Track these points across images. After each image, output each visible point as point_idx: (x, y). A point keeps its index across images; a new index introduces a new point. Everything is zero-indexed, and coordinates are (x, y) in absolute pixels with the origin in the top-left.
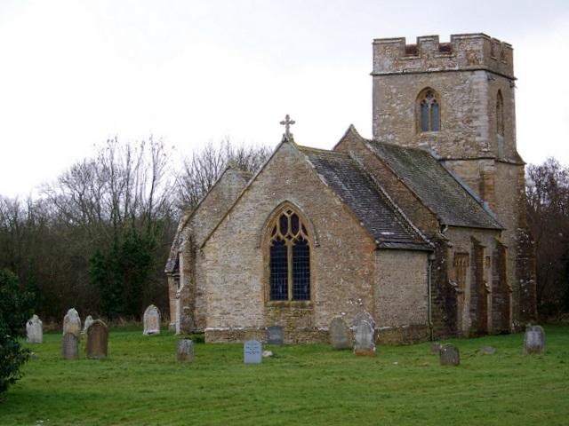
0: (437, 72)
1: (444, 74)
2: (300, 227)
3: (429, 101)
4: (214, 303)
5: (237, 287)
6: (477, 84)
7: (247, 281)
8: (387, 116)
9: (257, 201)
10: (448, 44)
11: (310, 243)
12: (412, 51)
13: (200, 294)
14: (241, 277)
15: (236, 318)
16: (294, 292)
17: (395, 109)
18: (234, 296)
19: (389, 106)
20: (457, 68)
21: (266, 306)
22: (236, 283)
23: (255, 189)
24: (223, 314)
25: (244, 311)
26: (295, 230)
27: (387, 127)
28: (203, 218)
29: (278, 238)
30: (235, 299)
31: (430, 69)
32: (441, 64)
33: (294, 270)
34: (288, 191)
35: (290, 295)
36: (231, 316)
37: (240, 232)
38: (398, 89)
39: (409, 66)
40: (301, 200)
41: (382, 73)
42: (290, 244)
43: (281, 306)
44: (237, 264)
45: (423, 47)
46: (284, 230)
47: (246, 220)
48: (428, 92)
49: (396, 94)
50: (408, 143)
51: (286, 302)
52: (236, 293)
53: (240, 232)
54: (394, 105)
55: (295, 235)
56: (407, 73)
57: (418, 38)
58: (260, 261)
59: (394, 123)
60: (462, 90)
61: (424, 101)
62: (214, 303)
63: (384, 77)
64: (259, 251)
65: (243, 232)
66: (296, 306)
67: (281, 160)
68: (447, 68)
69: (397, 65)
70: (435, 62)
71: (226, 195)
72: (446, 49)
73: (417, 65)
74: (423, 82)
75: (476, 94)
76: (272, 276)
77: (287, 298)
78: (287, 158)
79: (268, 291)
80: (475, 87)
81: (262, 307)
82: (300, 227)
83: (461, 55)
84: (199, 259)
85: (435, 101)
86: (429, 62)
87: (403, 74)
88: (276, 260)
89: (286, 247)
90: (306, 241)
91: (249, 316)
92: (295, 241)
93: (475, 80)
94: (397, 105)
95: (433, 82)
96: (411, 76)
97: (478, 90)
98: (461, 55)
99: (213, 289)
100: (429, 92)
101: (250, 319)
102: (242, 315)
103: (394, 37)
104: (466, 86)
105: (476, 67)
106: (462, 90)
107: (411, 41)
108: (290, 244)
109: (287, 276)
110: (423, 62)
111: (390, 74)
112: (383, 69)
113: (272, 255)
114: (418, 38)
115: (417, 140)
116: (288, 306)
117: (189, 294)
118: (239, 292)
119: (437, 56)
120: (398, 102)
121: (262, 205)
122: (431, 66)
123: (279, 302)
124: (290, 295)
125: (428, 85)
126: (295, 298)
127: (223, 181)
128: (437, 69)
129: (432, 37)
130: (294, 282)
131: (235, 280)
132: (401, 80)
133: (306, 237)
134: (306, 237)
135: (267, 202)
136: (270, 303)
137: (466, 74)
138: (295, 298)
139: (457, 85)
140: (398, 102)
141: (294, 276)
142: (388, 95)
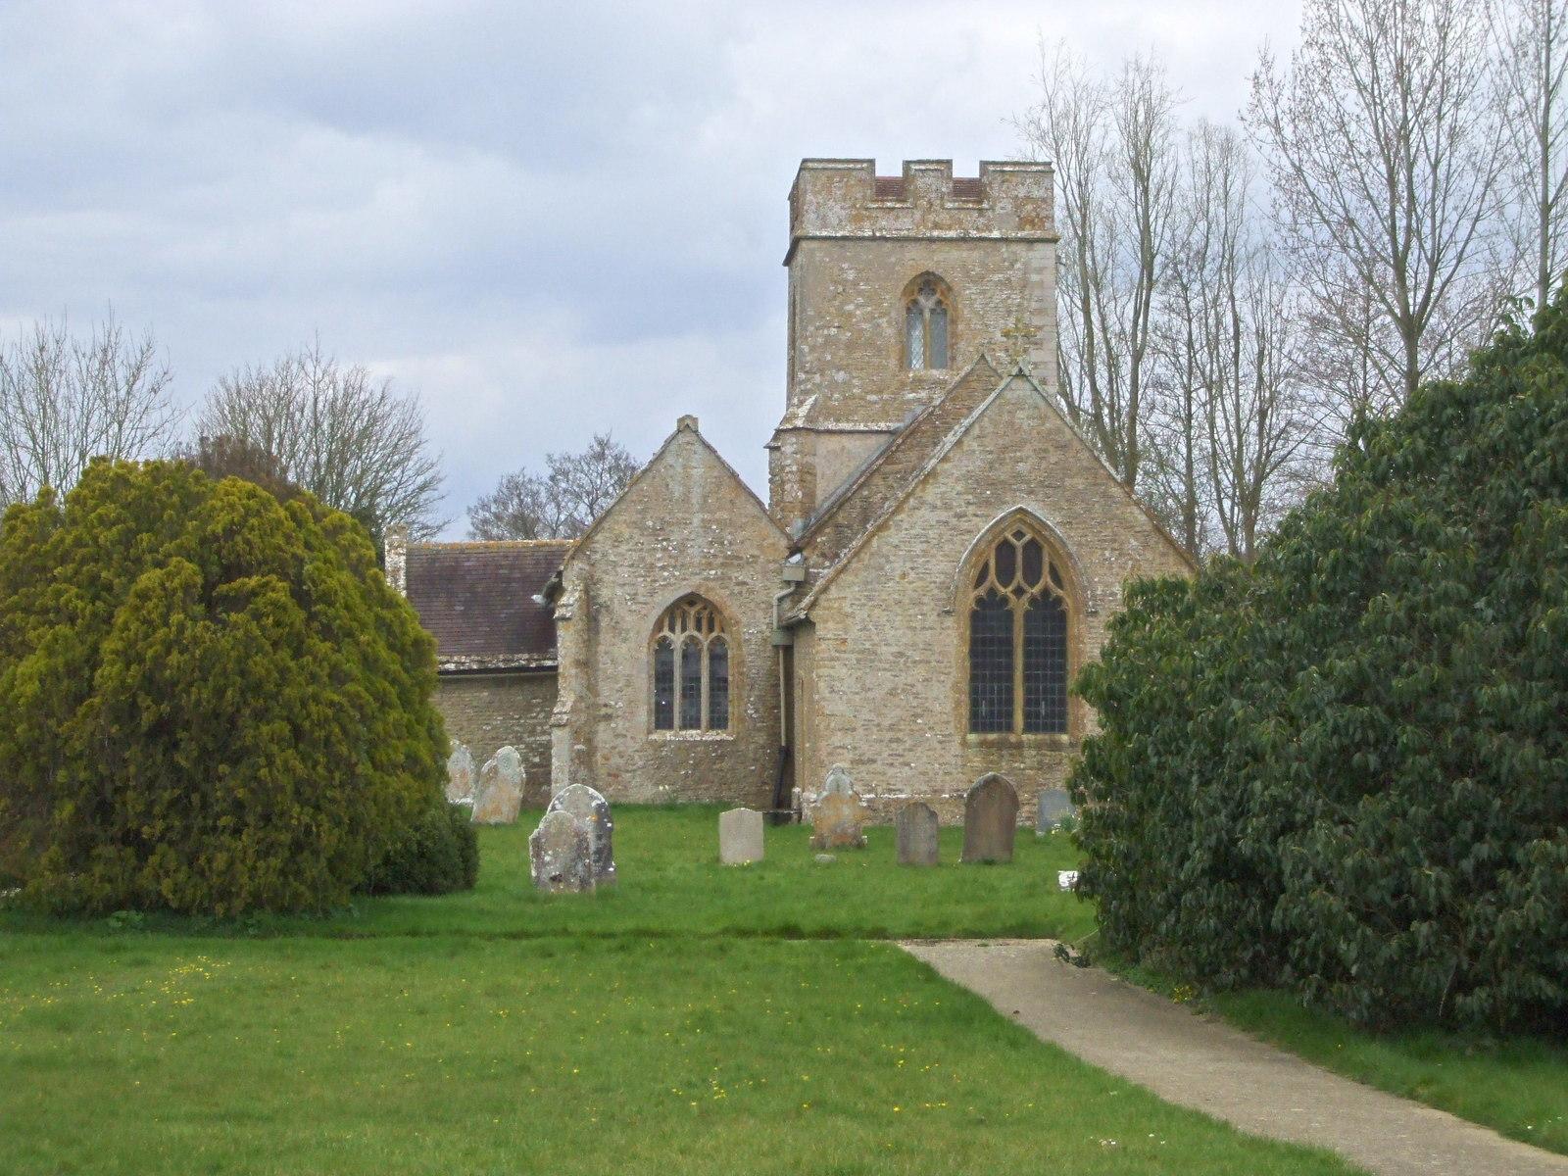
0: (951, 240)
1: (965, 246)
2: (1046, 569)
3: (927, 303)
4: (838, 739)
5: (896, 701)
6: (1040, 270)
7: (919, 687)
8: (833, 331)
9: (947, 507)
10: (971, 181)
11: (1069, 603)
12: (888, 189)
13: (608, 717)
14: (904, 679)
15: (891, 771)
16: (1027, 715)
17: (851, 315)
18: (886, 723)
19: (840, 309)
20: (996, 234)
21: (964, 744)
22: (892, 693)
23: (941, 479)
24: (858, 762)
25: (909, 756)
26: (1032, 576)
27: (833, 354)
28: (617, 541)
29: (992, 591)
30: (891, 728)
31: (936, 233)
32: (960, 222)
33: (1027, 666)
34: (1024, 487)
35: (1019, 719)
36: (878, 766)
37: (904, 576)
38: (859, 271)
39: (887, 225)
40: (1056, 507)
41: (824, 234)
42: (1020, 606)
43: (1000, 745)
44: (895, 649)
45: (920, 183)
46: (1005, 575)
47: (918, 548)
48: (928, 282)
49: (855, 283)
50: (881, 392)
51: (1013, 738)
52: (891, 716)
53: (904, 576)
54: (851, 307)
55: (1032, 585)
56: (884, 239)
57: (907, 164)
58: (952, 641)
59: (851, 346)
60: (1007, 283)
61: (915, 302)
62: (838, 739)
63: (826, 245)
64: (949, 622)
65: (912, 575)
66: (1038, 746)
67: (1006, 417)
68: (974, 233)
69: (857, 219)
70: (944, 218)
71: (678, 491)
72: (971, 191)
73: (904, 225)
74: (917, 260)
75: (1037, 292)
76: (974, 678)
77: (1010, 728)
78: (1020, 414)
79: (965, 711)
80: (1034, 277)
81: (955, 747)
82: (1046, 569)
83: (1004, 206)
84: (605, 637)
85: (939, 302)
86: (931, 217)
87: (873, 238)
88: (984, 641)
89: (1010, 615)
90: (1059, 601)
91: (921, 769)
92: (1033, 601)
93: (1035, 264)
94: (858, 306)
95: (944, 261)
96: (889, 245)
97: (1041, 284)
98: (1004, 206)
99: (835, 706)
100: (927, 283)
101: (924, 774)
102: (908, 765)
103: (826, 156)
104: (1015, 275)
105: (1038, 234)
106: (1007, 283)
107: (889, 168)
108: (1020, 606)
109: (1010, 678)
110: (918, 215)
111: (844, 238)
112: (825, 226)
113: (974, 629)
114: (907, 164)
115: (903, 385)
116: (1019, 746)
117: (583, 717)
118: (898, 712)
119: (949, 205)
120: (861, 300)
121: (959, 516)
122: (936, 226)
123: (992, 737)
124: (1019, 719)
125: (930, 266)
126: (1029, 728)
127: (670, 459)
128: (952, 234)
129: (939, 162)
130: (1028, 691)
131: (889, 685)
132: (867, 253)
133: (1060, 592)
134: (1060, 592)
135: (971, 509)
136: (972, 737)
137: (1014, 247)
138: (1029, 728)
139: (994, 271)
140: (861, 300)
141: (1027, 678)
142: (835, 283)
